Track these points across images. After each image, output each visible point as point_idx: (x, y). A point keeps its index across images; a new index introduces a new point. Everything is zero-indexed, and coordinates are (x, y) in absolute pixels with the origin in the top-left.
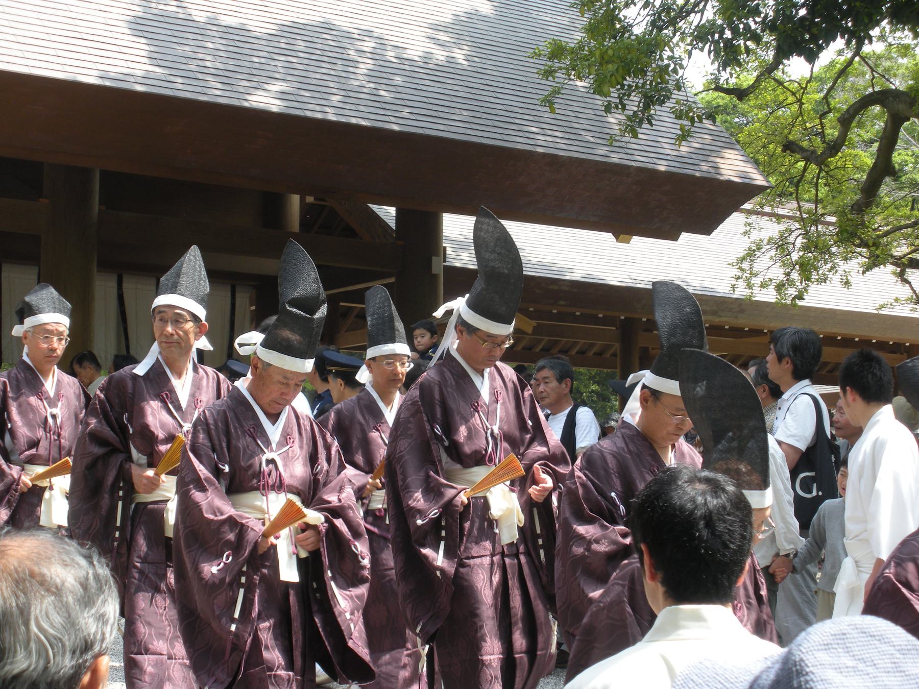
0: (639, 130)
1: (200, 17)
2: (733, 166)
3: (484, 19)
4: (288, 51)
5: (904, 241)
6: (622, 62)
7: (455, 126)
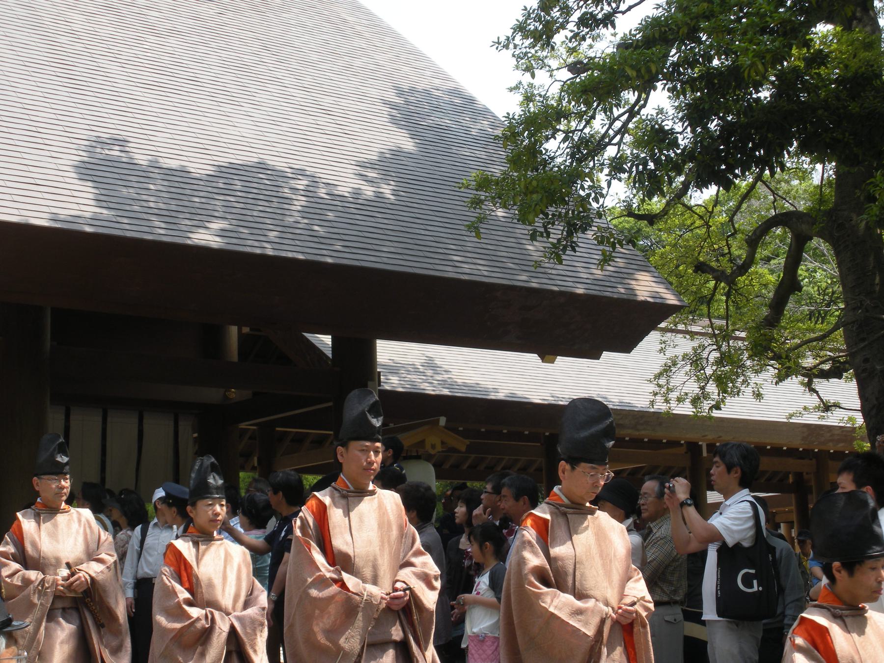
0: (564, 257)
1: (142, 159)
2: (646, 287)
3: (409, 155)
4: (228, 191)
5: (810, 353)
6: (546, 192)
7: (385, 257)
